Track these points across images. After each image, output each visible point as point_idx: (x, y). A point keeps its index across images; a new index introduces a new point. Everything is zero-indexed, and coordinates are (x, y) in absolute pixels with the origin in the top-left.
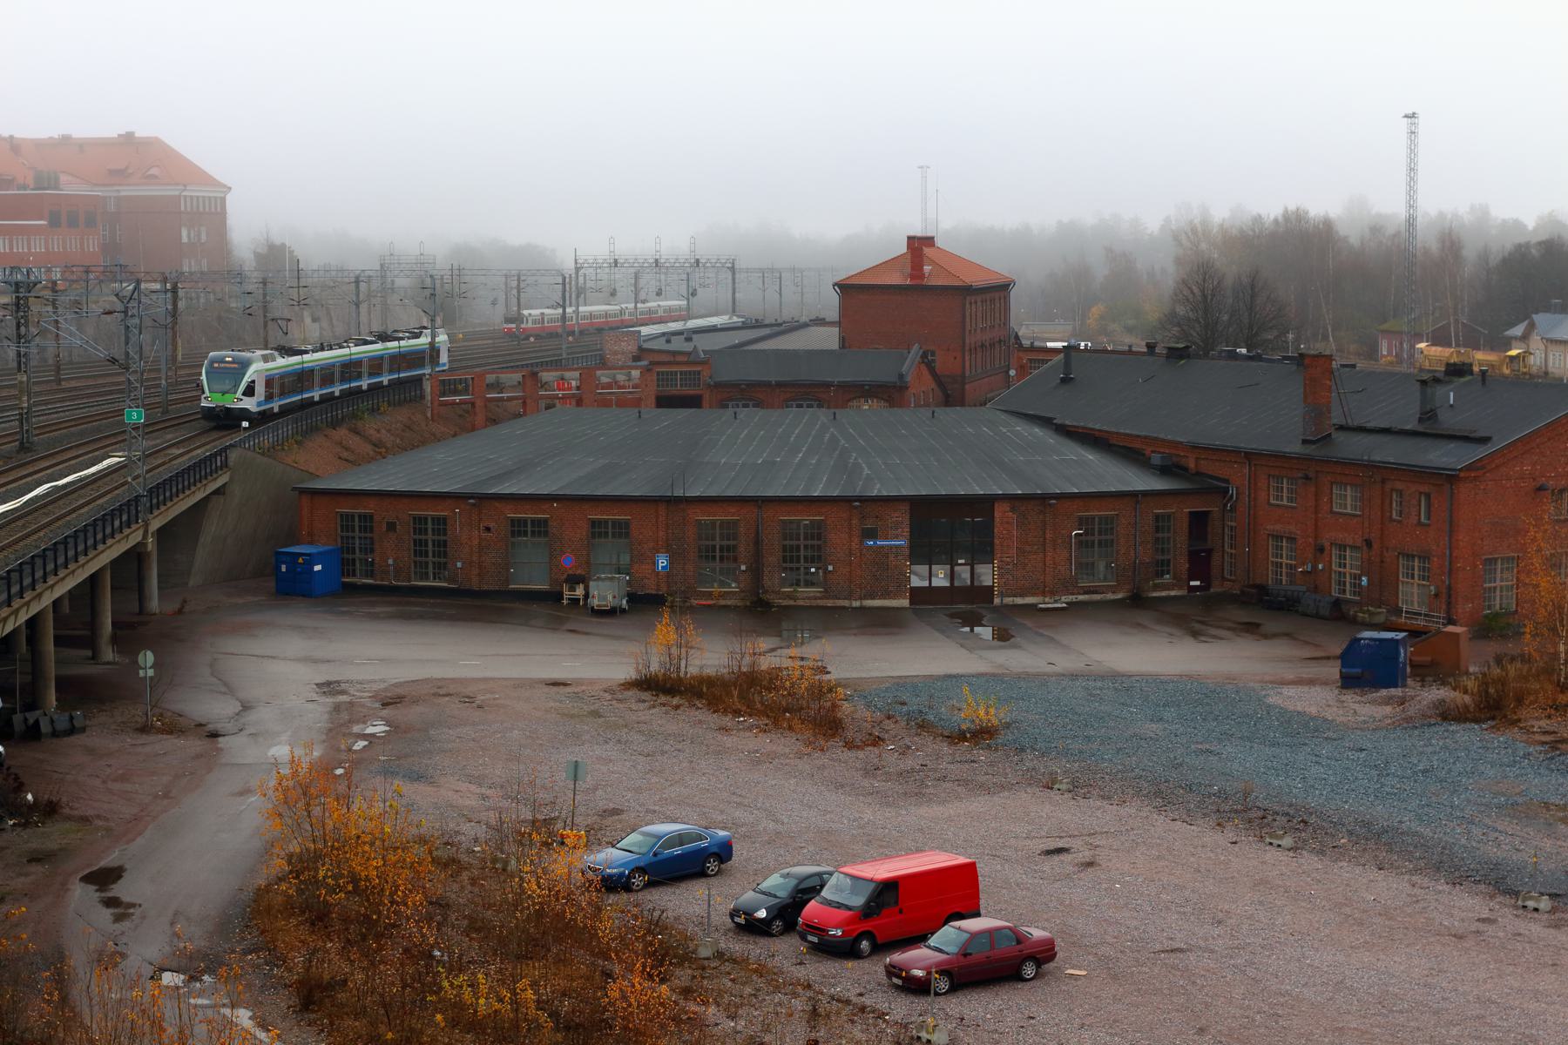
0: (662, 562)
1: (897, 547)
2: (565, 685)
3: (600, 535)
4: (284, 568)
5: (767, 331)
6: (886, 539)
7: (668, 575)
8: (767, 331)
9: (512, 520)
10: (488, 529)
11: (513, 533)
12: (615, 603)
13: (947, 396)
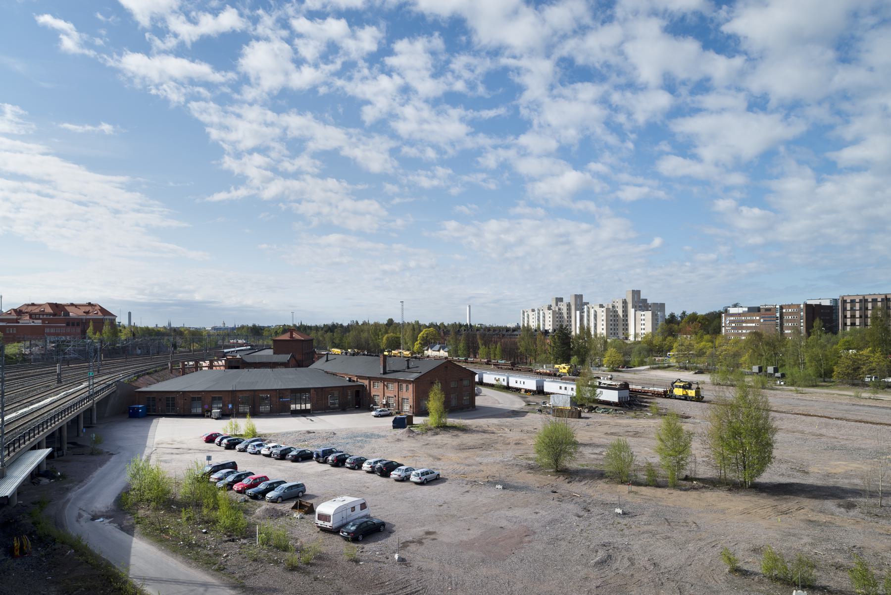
0: (230, 406)
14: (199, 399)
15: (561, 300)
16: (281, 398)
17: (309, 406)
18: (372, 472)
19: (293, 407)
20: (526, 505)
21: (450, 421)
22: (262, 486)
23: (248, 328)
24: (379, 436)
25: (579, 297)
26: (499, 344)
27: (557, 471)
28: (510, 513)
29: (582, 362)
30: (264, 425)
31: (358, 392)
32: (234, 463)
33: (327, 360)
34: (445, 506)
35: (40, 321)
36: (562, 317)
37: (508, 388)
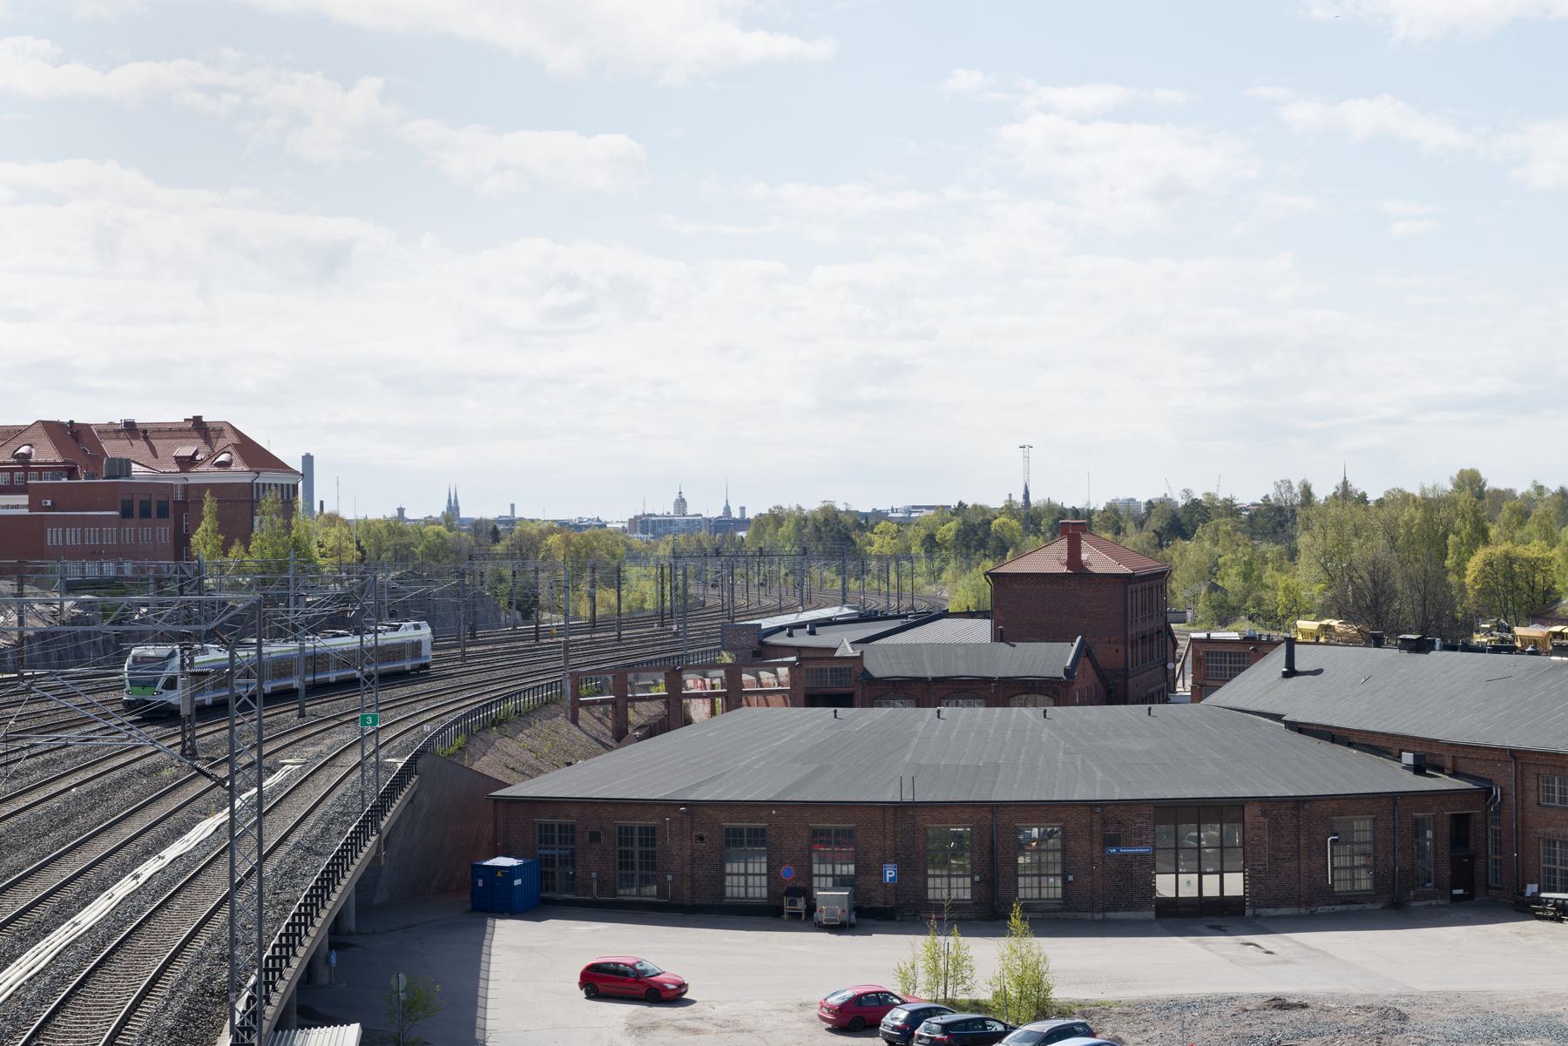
0: (890, 873)
1: (1141, 855)
2: (1304, 1006)
3: (735, 842)
4: (480, 883)
5: (897, 623)
6: (1130, 846)
7: (896, 887)
8: (897, 623)
9: (727, 830)
10: (701, 839)
11: (727, 842)
12: (845, 917)
13: (1110, 692)
14: (757, 837)
16: (1114, 841)
17: (1235, 884)
19: (1165, 885)
23: (802, 521)
31: (1460, 824)
33: (1291, 672)
35: (23, 499)
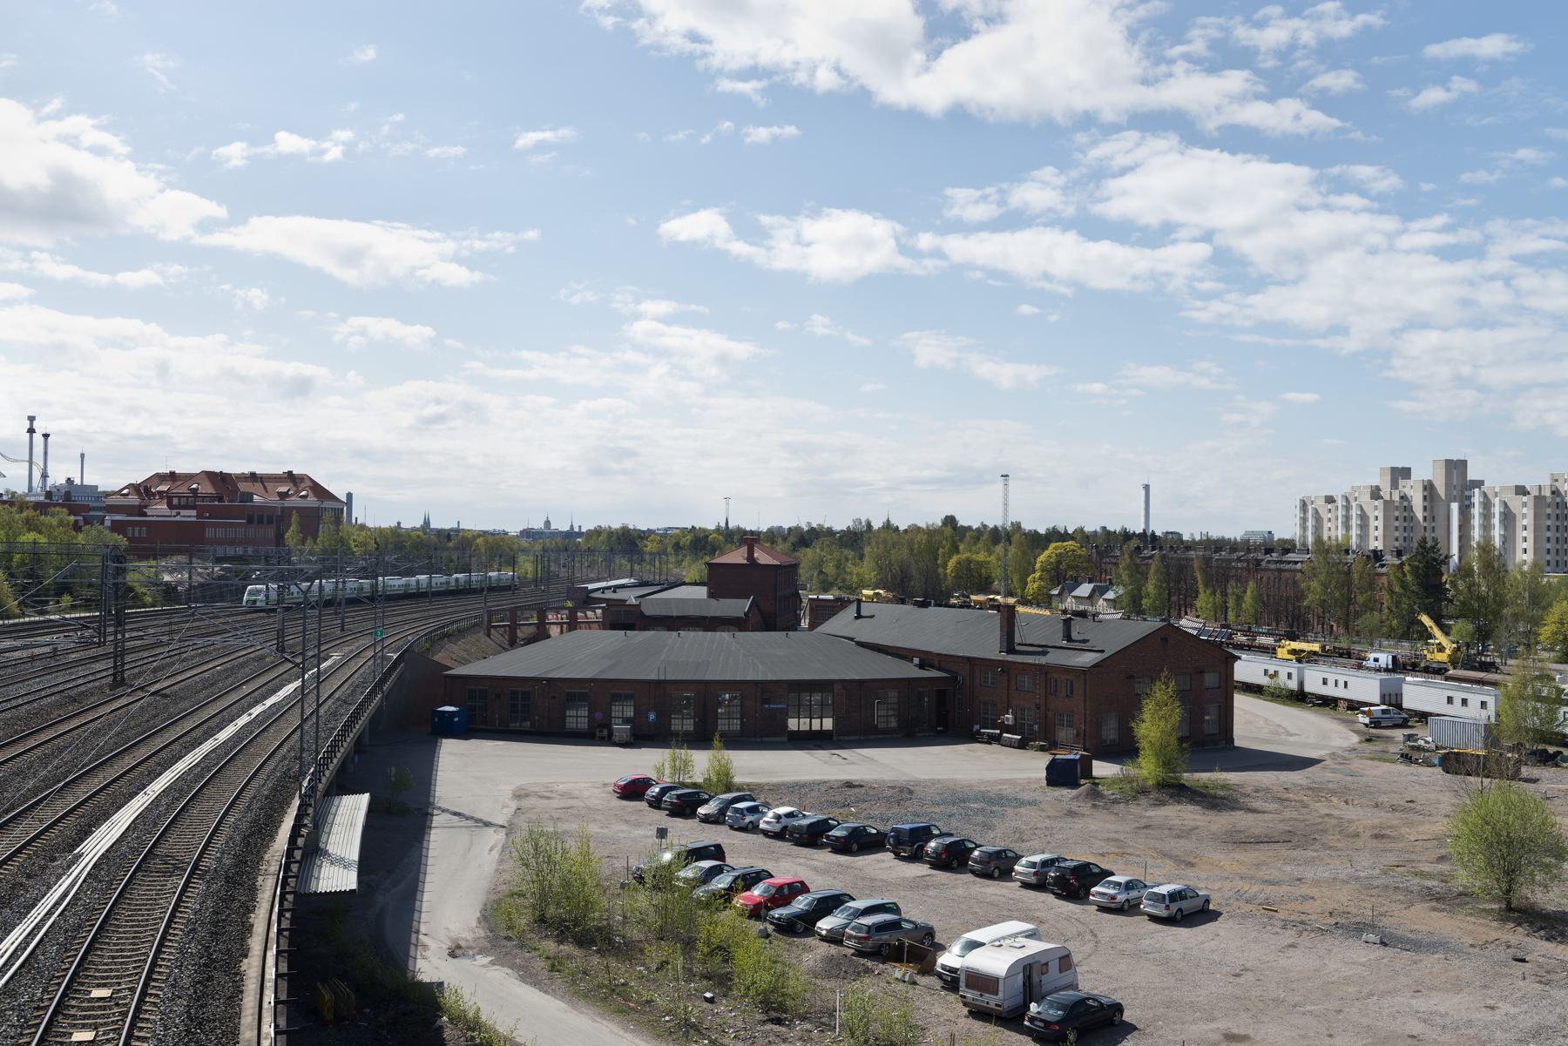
0: (652, 717)
15: (1405, 473)
17: (828, 724)
18: (1039, 885)
19: (793, 724)
20: (1458, 986)
21: (1190, 778)
22: (801, 904)
23: (610, 533)
24: (1022, 803)
25: (1456, 468)
26: (1251, 584)
27: (1510, 909)
28: (1421, 1004)
29: (1484, 635)
30: (753, 766)
32: (718, 847)
33: (859, 616)
34: (1249, 976)
35: (194, 513)
36: (1409, 516)
37: (1299, 697)
